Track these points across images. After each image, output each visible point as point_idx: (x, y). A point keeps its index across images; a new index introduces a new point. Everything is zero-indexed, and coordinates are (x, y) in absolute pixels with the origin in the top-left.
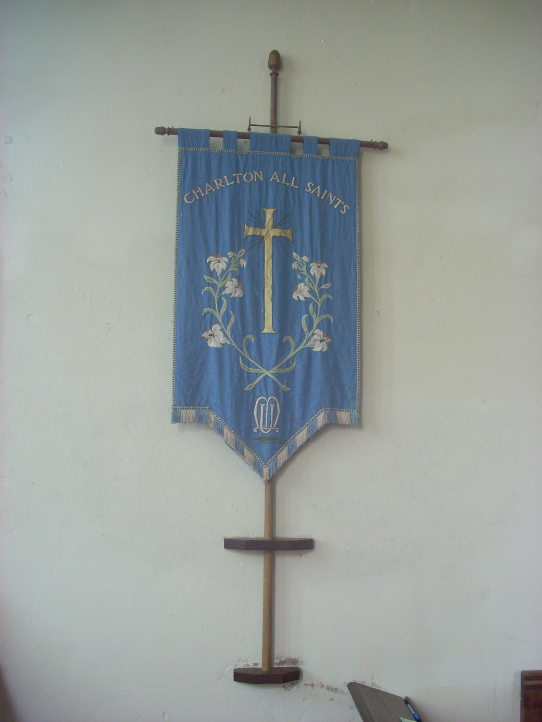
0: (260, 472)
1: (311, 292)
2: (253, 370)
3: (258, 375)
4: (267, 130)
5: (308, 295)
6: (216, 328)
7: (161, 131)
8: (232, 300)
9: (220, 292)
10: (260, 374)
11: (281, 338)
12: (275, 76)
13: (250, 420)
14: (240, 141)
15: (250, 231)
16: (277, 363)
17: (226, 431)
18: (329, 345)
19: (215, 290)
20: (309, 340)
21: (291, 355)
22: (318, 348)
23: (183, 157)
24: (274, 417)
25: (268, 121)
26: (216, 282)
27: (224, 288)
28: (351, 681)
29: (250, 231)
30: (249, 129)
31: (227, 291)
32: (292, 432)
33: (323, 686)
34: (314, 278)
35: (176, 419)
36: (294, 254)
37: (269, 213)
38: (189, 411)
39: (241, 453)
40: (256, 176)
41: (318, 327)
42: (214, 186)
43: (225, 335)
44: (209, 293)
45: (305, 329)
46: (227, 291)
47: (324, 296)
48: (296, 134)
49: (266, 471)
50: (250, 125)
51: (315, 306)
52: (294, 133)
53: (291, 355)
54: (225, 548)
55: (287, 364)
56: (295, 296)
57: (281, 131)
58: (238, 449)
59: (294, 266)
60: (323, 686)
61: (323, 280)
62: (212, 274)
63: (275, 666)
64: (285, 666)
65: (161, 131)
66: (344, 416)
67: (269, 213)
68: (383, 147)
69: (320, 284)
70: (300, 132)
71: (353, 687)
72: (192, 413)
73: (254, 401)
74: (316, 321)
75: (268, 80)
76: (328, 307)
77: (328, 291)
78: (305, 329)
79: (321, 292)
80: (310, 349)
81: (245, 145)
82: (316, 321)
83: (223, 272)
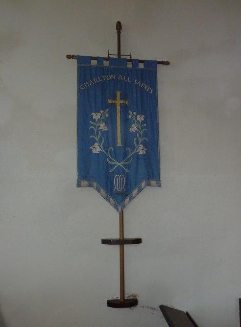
0: (117, 209)
1: (138, 128)
2: (113, 163)
3: (115, 165)
4: (116, 57)
5: (136, 129)
6: (96, 144)
7: (69, 57)
8: (103, 133)
9: (98, 128)
10: (116, 165)
11: (125, 150)
12: (119, 33)
13: (112, 185)
14: (104, 61)
15: (109, 101)
16: (123, 159)
17: (101, 191)
18: (146, 151)
19: (95, 128)
20: (137, 149)
21: (130, 156)
22: (141, 153)
23: (79, 68)
24: (123, 184)
25: (117, 53)
26: (95, 124)
27: (99, 126)
28: (161, 304)
29: (109, 101)
30: (108, 56)
31: (100, 128)
32: (131, 191)
33: (148, 307)
34: (139, 122)
35: (79, 185)
36: (130, 112)
37: (118, 93)
38: (84, 182)
39: (108, 200)
40: (112, 77)
41: (142, 143)
42: (93, 81)
43: (100, 148)
44: (92, 129)
45: (135, 144)
46: (100, 128)
47: (144, 130)
48: (129, 58)
49: (120, 208)
50: (109, 54)
51: (140, 135)
52: (128, 58)
53: (130, 156)
54: (137, 299)
55: (128, 160)
56: (130, 130)
57: (122, 57)
58: (107, 199)
59: (130, 117)
60: (148, 307)
61: (143, 123)
62: (94, 121)
63: (126, 298)
64: (131, 298)
65: (69, 57)
66: (153, 183)
67: (118, 93)
68: (167, 63)
69: (142, 125)
70: (131, 58)
71: (163, 308)
72: (85, 183)
73: (114, 177)
74: (140, 141)
75: (116, 35)
76: (145, 134)
77: (145, 127)
78: (135, 144)
79: (142, 128)
80: (137, 153)
81: (106, 63)
82: (140, 141)
83: (99, 119)
